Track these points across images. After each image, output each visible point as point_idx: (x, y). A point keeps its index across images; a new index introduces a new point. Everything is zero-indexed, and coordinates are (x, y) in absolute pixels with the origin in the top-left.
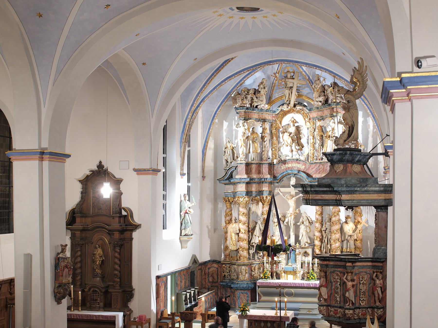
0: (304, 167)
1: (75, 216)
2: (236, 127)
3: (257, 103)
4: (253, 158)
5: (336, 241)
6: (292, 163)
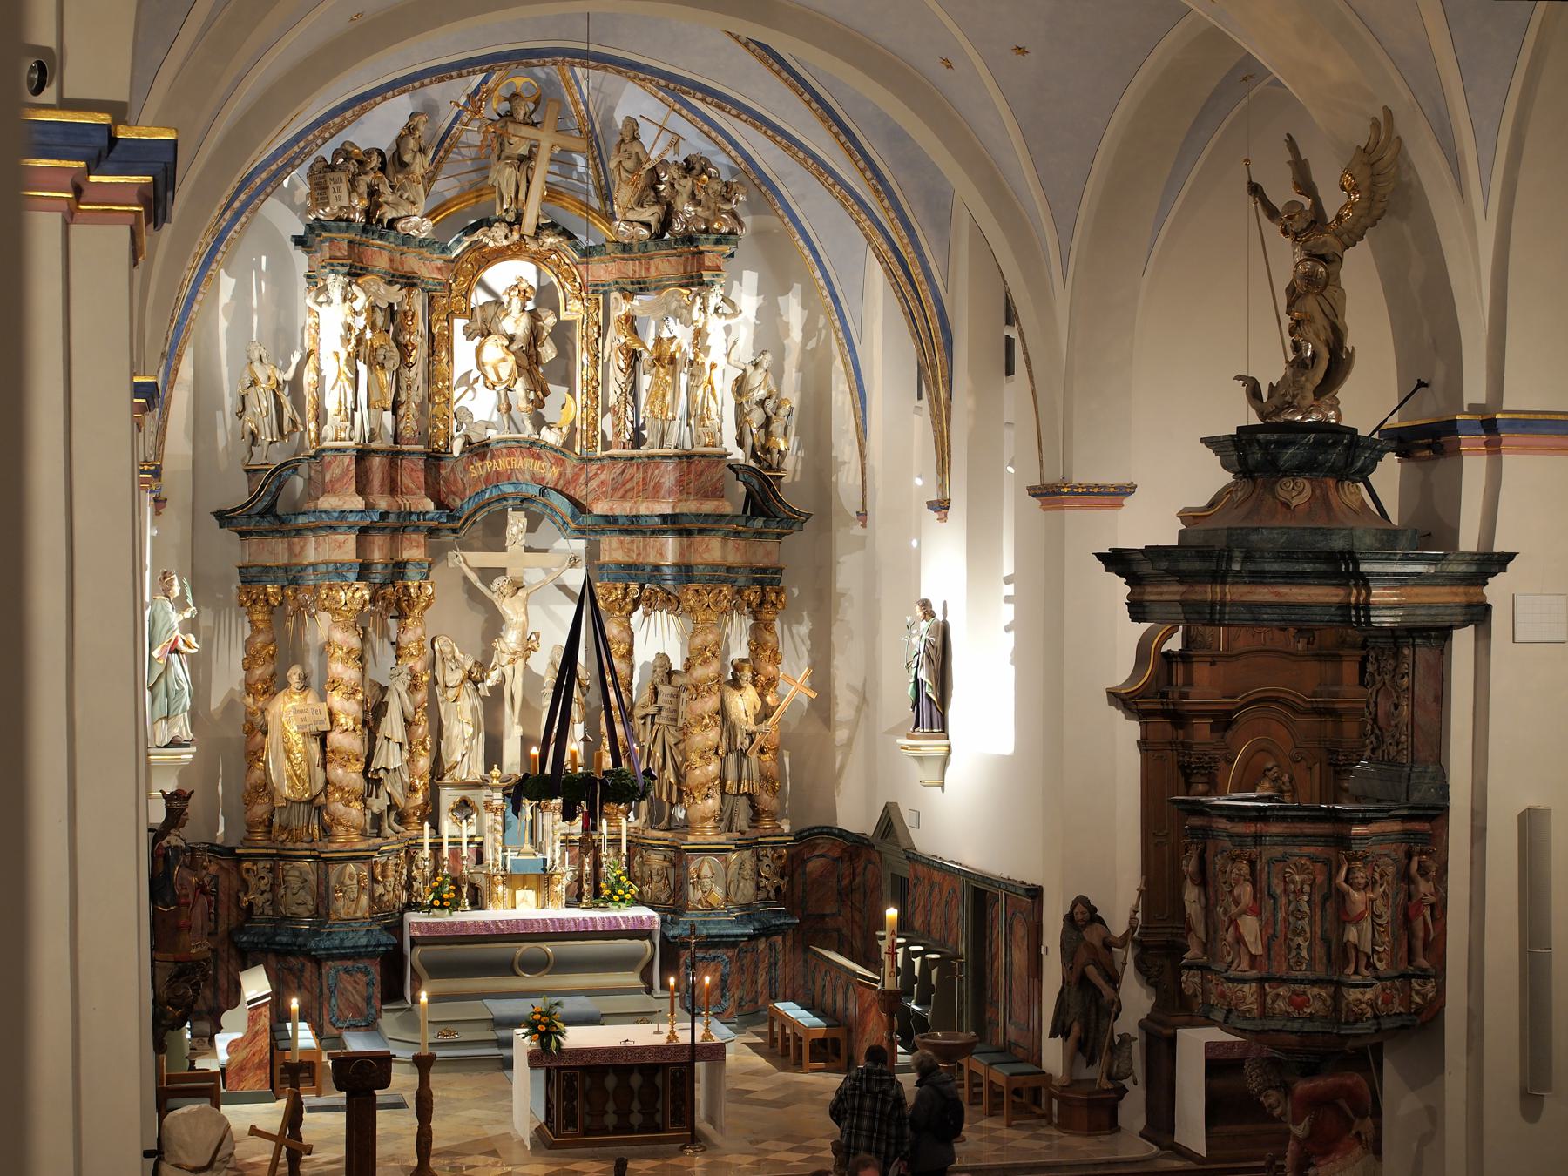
0: (556, 470)
2: (316, 302)
3: (394, 211)
4: (372, 430)
6: (510, 456)
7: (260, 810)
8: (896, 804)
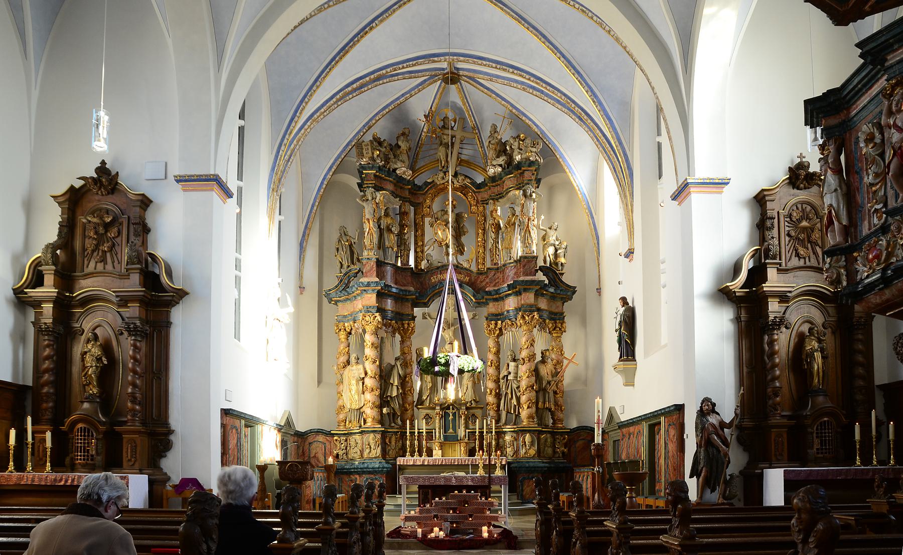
1: (41, 271)
7: (342, 416)
8: (614, 407)
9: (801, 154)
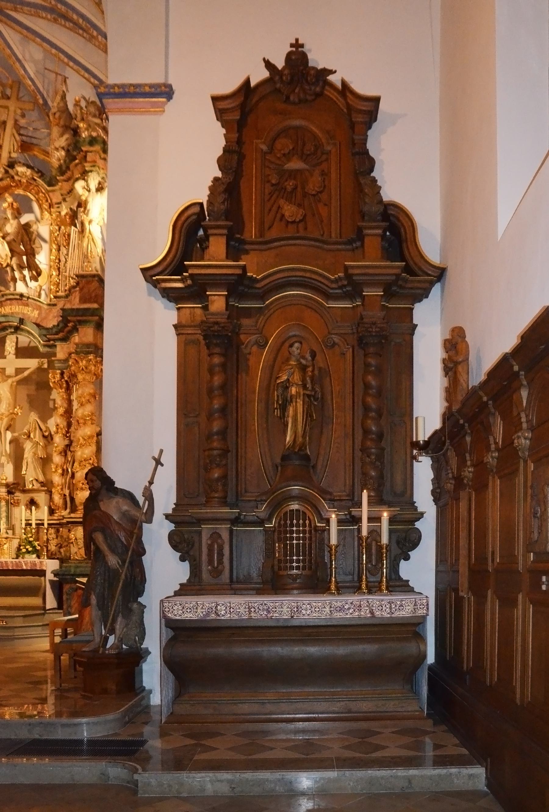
5: (84, 463)
9: (297, 40)
